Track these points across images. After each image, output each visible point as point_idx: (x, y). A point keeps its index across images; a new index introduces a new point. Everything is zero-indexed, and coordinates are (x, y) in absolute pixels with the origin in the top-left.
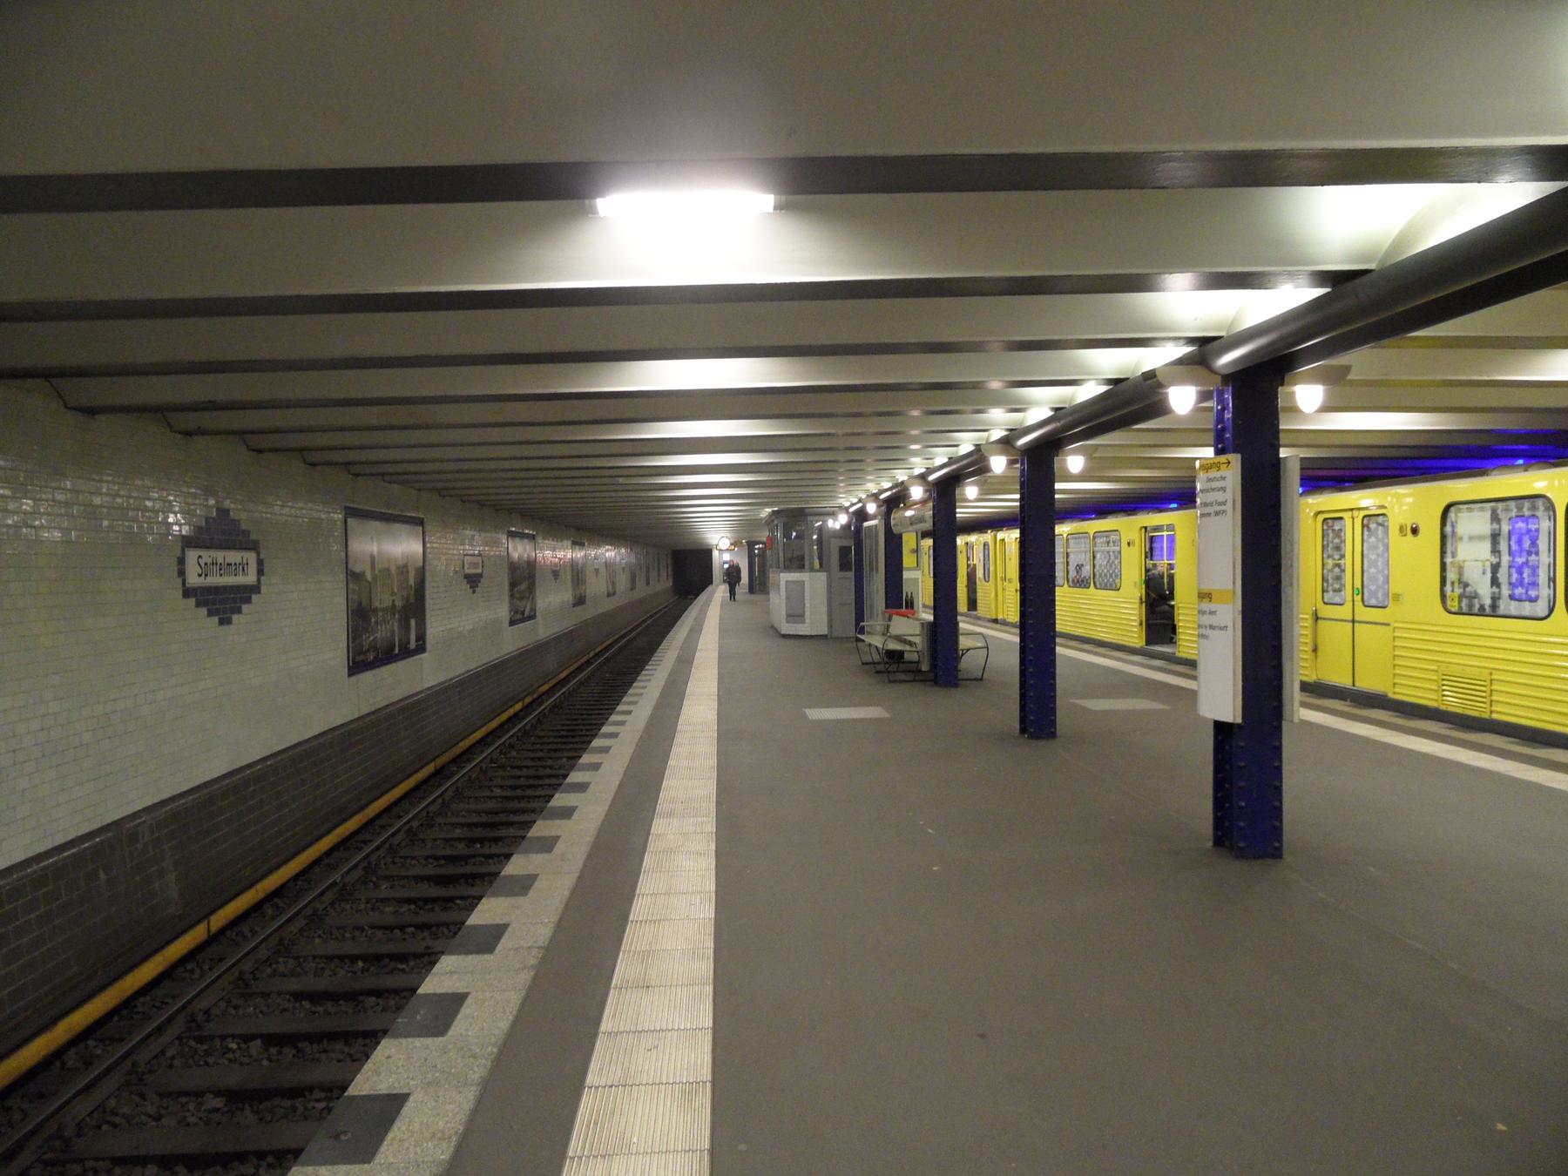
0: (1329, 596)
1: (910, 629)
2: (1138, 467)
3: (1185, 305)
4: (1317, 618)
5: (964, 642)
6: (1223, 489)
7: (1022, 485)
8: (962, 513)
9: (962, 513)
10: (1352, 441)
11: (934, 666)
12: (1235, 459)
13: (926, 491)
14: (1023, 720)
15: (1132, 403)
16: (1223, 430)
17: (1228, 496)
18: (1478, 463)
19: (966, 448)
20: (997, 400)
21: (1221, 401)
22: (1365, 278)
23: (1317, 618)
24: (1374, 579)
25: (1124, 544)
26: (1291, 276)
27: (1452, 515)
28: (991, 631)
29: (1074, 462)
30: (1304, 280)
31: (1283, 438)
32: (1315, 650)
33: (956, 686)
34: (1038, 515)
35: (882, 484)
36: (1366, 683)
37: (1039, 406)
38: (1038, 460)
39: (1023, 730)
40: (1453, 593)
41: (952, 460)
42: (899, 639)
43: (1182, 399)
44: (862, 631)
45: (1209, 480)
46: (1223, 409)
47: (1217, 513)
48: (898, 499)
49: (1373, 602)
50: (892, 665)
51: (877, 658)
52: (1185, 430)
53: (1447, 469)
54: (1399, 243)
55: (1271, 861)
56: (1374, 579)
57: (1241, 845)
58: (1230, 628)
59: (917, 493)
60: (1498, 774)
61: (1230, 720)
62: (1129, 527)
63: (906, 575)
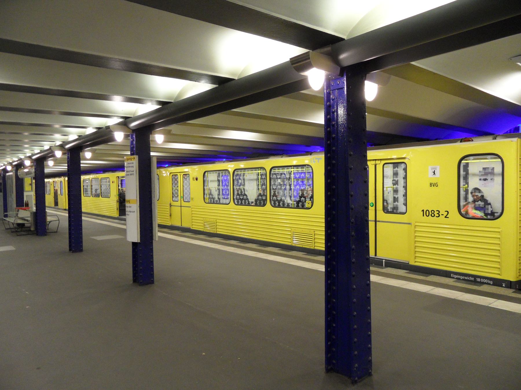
0: (174, 198)
1: (26, 215)
2: (112, 157)
3: (119, 106)
4: (171, 206)
5: (49, 219)
6: (133, 167)
7: (68, 162)
8: (47, 171)
9: (47, 171)
10: (177, 152)
11: (36, 228)
12: (136, 157)
13: (31, 162)
14: (70, 246)
15: (102, 137)
16: (133, 147)
17: (135, 168)
18: (215, 159)
19: (46, 147)
20: (58, 131)
21: (132, 138)
22: (169, 104)
23: (171, 206)
24: (186, 193)
25: (111, 182)
26: (151, 101)
27: (206, 174)
28: (57, 215)
29: (88, 155)
30: (155, 103)
31: (151, 149)
32: (170, 216)
33: (46, 235)
34: (74, 172)
35: (15, 159)
36: (185, 225)
37: (73, 135)
38: (74, 153)
39: (70, 250)
40: (207, 197)
41: (41, 152)
42: (22, 219)
43: (119, 136)
44: (6, 216)
45: (128, 163)
46: (133, 140)
47: (131, 174)
48: (20, 166)
49: (186, 200)
50: (20, 229)
51: (12, 226)
52: (120, 145)
53: (206, 161)
54: (179, 95)
55: (150, 285)
56: (186, 193)
57: (141, 281)
58: (136, 212)
59: (28, 163)
60: (217, 249)
61: (136, 241)
62: (112, 176)
63: (25, 194)
